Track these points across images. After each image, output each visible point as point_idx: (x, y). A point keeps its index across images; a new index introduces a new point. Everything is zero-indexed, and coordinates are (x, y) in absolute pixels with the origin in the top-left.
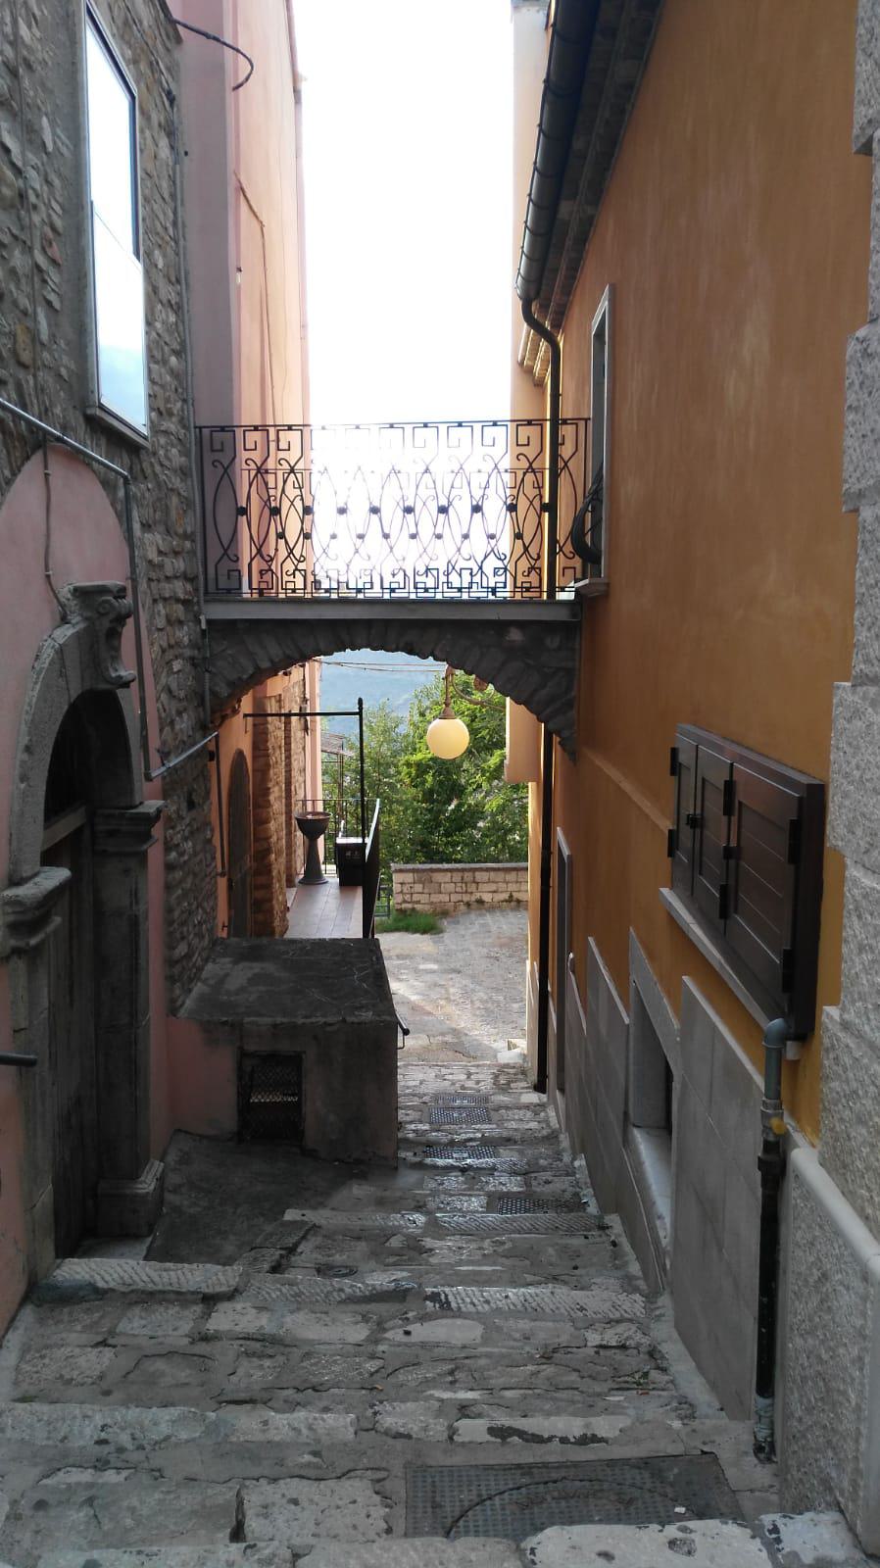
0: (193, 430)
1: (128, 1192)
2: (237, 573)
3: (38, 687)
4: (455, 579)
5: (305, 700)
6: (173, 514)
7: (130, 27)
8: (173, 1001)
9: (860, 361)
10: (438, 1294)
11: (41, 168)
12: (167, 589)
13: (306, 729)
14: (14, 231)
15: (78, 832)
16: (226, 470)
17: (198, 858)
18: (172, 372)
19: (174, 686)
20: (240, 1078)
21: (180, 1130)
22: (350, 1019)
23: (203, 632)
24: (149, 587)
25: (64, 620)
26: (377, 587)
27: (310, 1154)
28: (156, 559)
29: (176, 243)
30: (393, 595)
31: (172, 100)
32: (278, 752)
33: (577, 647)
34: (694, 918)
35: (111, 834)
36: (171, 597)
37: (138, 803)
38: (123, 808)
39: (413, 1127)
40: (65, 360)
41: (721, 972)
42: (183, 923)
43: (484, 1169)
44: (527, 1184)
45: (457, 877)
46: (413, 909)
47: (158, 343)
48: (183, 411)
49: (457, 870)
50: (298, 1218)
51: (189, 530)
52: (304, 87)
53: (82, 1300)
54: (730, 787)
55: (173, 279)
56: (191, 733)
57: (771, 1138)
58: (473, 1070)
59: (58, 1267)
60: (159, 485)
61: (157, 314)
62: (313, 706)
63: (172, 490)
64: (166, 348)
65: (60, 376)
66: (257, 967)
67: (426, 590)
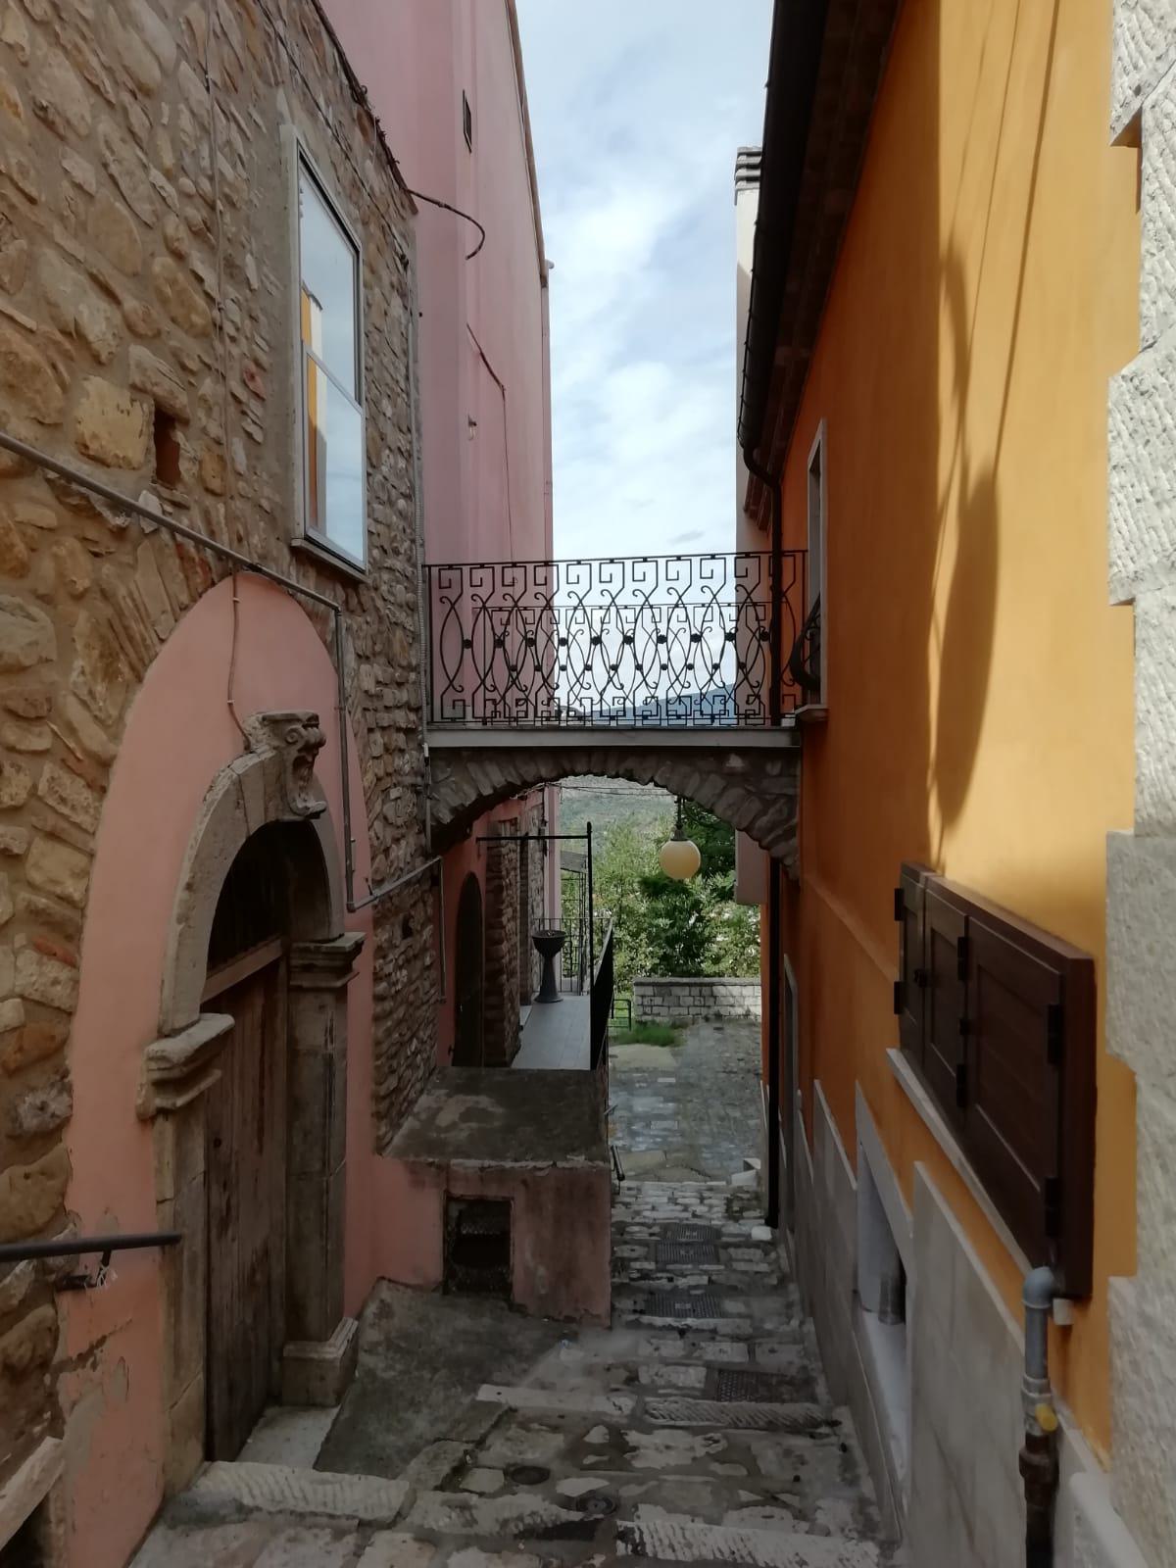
0: (420, 568)
1: (315, 1356)
2: (461, 703)
3: (207, 820)
4: (707, 710)
5: (544, 822)
6: (397, 647)
7: (359, 189)
8: (379, 1139)
9: (1130, 404)
10: (632, 1530)
11: (245, 304)
12: (385, 719)
13: (544, 850)
14: (207, 360)
15: (273, 967)
16: (453, 606)
17: (413, 987)
18: (401, 514)
19: (391, 815)
20: (446, 1224)
21: (383, 1278)
22: (560, 1164)
23: (426, 759)
24: (364, 716)
25: (248, 749)
26: (630, 715)
27: (519, 1310)
28: (373, 689)
29: (408, 395)
30: (645, 722)
31: (405, 265)
32: (513, 873)
33: (798, 773)
34: (927, 1092)
35: (308, 968)
36: (390, 726)
37: (336, 935)
38: (319, 942)
39: (637, 1265)
40: (267, 491)
41: (960, 1172)
42: (395, 1056)
43: (703, 1331)
44: (751, 1352)
45: (695, 991)
46: (653, 1022)
47: (383, 486)
48: (411, 550)
49: (695, 984)
50: (493, 1398)
51: (414, 663)
52: (552, 275)
53: (222, 1521)
54: (964, 944)
55: (405, 429)
56: (409, 859)
57: (1037, 1433)
58: (706, 1194)
59: (205, 1473)
60: (381, 619)
61: (384, 458)
62: (552, 829)
63: (396, 624)
64: (393, 492)
65: (260, 506)
66: (471, 1100)
67: (679, 717)
